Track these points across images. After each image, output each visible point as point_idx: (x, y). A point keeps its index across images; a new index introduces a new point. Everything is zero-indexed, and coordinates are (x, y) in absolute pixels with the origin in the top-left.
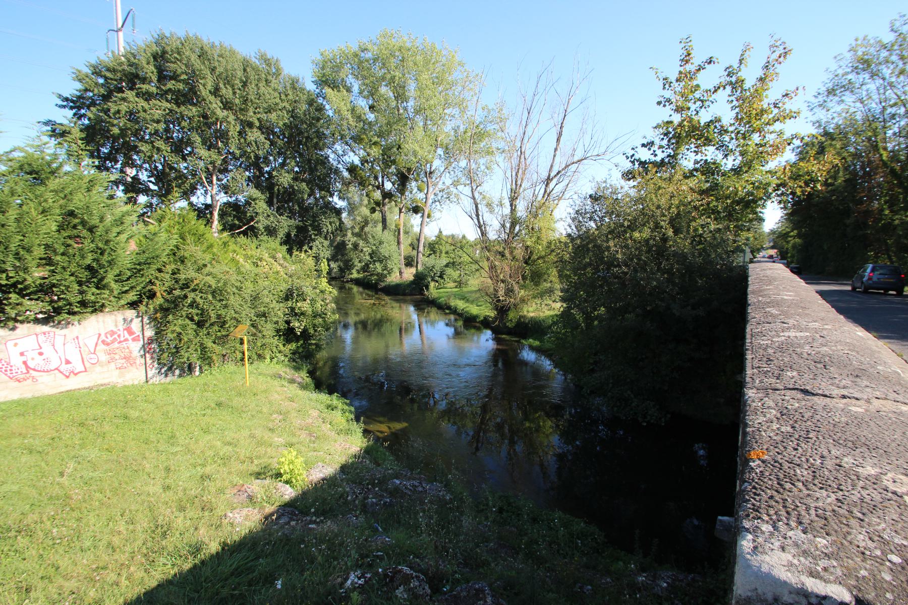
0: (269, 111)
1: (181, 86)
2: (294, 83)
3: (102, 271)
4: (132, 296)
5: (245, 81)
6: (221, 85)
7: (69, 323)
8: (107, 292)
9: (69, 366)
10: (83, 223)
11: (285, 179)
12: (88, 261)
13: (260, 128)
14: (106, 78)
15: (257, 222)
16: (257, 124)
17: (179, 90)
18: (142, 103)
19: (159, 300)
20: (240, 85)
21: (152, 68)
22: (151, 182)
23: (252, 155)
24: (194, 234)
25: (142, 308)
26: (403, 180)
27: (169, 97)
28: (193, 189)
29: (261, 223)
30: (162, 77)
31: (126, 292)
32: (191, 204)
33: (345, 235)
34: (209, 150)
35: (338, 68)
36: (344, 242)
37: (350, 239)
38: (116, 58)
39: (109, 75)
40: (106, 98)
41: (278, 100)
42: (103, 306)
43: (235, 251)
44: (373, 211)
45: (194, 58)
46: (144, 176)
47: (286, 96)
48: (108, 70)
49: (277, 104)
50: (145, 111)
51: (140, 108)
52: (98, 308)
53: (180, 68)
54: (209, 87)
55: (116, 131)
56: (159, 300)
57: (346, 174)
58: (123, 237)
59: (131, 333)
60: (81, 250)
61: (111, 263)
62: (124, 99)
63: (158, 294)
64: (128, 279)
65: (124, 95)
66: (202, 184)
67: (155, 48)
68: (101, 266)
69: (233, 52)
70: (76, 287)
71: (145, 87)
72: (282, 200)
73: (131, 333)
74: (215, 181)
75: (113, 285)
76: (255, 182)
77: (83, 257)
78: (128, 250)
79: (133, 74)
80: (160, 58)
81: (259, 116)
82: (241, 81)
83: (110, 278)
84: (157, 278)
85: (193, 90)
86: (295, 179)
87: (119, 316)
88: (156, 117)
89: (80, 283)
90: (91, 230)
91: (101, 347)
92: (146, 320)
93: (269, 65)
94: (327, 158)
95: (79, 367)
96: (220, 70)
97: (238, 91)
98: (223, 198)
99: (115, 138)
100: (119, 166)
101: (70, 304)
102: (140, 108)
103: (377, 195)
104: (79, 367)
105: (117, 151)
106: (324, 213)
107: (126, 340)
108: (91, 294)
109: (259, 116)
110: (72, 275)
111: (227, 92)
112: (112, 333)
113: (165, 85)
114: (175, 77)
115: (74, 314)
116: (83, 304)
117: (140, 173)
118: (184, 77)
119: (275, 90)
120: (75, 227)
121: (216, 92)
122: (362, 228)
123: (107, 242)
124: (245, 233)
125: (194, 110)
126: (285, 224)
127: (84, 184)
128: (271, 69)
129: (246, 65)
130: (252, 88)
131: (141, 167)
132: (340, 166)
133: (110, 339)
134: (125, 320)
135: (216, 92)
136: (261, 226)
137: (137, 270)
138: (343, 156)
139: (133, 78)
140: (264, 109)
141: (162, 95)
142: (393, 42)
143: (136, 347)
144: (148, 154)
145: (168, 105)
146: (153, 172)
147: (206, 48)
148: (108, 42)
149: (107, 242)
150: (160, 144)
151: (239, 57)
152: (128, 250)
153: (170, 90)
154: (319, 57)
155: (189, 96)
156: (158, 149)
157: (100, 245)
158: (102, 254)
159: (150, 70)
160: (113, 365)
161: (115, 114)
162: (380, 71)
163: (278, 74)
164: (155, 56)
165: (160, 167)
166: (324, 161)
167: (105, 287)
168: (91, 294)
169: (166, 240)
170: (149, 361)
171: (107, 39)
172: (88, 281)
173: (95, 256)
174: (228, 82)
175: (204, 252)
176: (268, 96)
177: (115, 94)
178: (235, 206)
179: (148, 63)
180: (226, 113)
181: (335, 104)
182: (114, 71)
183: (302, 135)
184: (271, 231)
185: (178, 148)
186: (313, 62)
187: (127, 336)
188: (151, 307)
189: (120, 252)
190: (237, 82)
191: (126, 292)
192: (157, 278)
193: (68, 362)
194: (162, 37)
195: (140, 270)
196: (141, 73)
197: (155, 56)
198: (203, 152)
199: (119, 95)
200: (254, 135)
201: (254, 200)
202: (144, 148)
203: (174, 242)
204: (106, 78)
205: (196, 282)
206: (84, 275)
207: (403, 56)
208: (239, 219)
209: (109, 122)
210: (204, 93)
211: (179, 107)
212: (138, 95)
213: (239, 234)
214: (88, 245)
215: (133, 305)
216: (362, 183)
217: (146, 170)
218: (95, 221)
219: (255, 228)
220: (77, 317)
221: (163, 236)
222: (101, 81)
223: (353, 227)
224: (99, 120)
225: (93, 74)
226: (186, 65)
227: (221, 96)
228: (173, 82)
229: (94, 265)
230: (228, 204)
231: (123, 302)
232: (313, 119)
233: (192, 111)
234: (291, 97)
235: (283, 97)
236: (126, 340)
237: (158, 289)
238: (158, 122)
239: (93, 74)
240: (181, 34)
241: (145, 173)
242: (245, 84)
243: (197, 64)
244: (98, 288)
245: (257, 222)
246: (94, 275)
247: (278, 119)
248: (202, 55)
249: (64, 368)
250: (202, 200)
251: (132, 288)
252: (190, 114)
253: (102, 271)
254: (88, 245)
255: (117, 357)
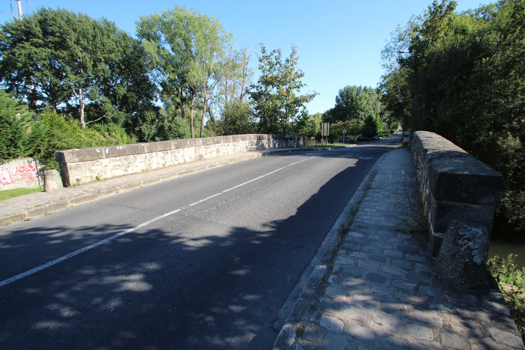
0: (110, 52)
1: (57, 39)
2: (125, 36)
3: (16, 141)
4: (30, 152)
5: (97, 34)
6: (81, 39)
7: (3, 163)
8: (19, 150)
9: (5, 180)
10: (6, 122)
11: (122, 91)
12: (10, 137)
13: (106, 62)
14: (12, 34)
15: (107, 115)
16: (103, 60)
17: (56, 41)
18: (34, 49)
19: (42, 153)
20: (92, 38)
21: (39, 29)
22: (43, 92)
23: (102, 77)
24: (58, 125)
25: (35, 156)
26: (193, 90)
27: (50, 46)
28: (69, 97)
29: (109, 116)
30: (46, 33)
31: (27, 150)
32: (68, 105)
33: (163, 122)
34: (76, 75)
35: (150, 27)
36: (163, 126)
37: (166, 124)
38: (17, 22)
39: (13, 32)
40: (14, 44)
41: (115, 46)
42: (18, 156)
43: (80, 132)
44: (177, 108)
45: (63, 23)
46: (39, 89)
47: (120, 43)
48: (13, 29)
49: (114, 49)
50: (36, 54)
51: (33, 52)
52: (15, 157)
53: (55, 29)
54: (73, 39)
55: (20, 65)
56: (42, 153)
57: (161, 88)
58: (24, 127)
59: (31, 167)
60: (6, 132)
61: (20, 137)
62: (23, 47)
63: (42, 151)
64: (28, 144)
65: (23, 45)
66: (74, 94)
67: (39, 17)
68: (16, 139)
69: (87, 18)
70: (5, 147)
71: (35, 40)
72: (123, 103)
73: (31, 167)
74: (81, 93)
75: (21, 147)
76: (106, 92)
77: (7, 135)
78: (28, 131)
79: (27, 31)
80: (43, 23)
81: (104, 55)
82: (93, 36)
83: (20, 144)
84: (41, 144)
85: (64, 40)
86: (129, 90)
87: (26, 160)
88: (43, 57)
89: (7, 146)
90: (10, 124)
91: (18, 173)
92: (38, 162)
93: (109, 26)
94: (148, 77)
95: (10, 181)
96: (79, 29)
97: (91, 42)
98: (87, 101)
99: (20, 69)
100: (23, 83)
101: (4, 154)
102: (33, 52)
103: (178, 100)
104: (10, 181)
105: (22, 75)
106: (147, 110)
107: (29, 170)
108: (12, 150)
109: (104, 55)
110: (3, 142)
111: (84, 42)
112: (23, 167)
113: (47, 38)
114: (53, 34)
115: (6, 159)
116: (9, 155)
117: (37, 88)
118: (58, 34)
119: (113, 40)
120: (3, 123)
121: (77, 42)
122: (173, 118)
123: (17, 129)
124: (100, 122)
125: (65, 53)
126: (123, 116)
127: (5, 105)
128: (109, 29)
129: (95, 26)
130: (98, 40)
131: (37, 84)
132: (156, 83)
133: (22, 170)
134: (28, 161)
135: (77, 42)
136: (109, 118)
137: (32, 140)
138: (156, 77)
139: (28, 34)
140: (107, 51)
141: (45, 45)
142: (181, 14)
143: (34, 174)
144: (40, 78)
145: (50, 51)
146: (44, 87)
147: (70, 17)
148: (11, 7)
149: (17, 129)
150: (47, 72)
151: (91, 21)
152: (28, 131)
153: (50, 42)
154: (140, 20)
155: (62, 45)
156: (46, 75)
157: (14, 130)
158: (16, 134)
159: (38, 30)
160: (24, 181)
161: (19, 55)
162: (174, 29)
163: (114, 31)
164: (40, 22)
165: (49, 84)
166: (146, 79)
167: (18, 147)
168: (12, 150)
169: (44, 128)
170: (40, 179)
171: (11, 5)
172: (10, 146)
173: (13, 135)
174: (84, 37)
175: (62, 132)
176: (109, 44)
177: (18, 44)
178: (96, 106)
179: (36, 26)
180: (84, 54)
181: (149, 47)
182: (16, 29)
183: (131, 64)
184: (115, 120)
185: (58, 74)
186: (136, 23)
187: (29, 168)
188: (39, 156)
189: (23, 133)
190: (90, 36)
191: (27, 150)
192: (41, 144)
193: (4, 179)
194: (44, 10)
195: (33, 141)
196: (32, 32)
197: (40, 22)
198: (72, 77)
199: (21, 45)
200: (103, 66)
201: (104, 103)
202: (38, 74)
203: (48, 128)
204: (12, 34)
205: (58, 145)
206: (9, 143)
207: (188, 22)
208: (98, 113)
209: (15, 60)
210: (70, 43)
211: (56, 51)
212: (31, 45)
213: (96, 122)
214: (9, 130)
215: (31, 156)
216: (168, 93)
217: (40, 86)
218: (11, 120)
219: (106, 118)
220: (7, 160)
221: (43, 126)
222: (9, 35)
223: (168, 117)
224: (9, 59)
225: (4, 31)
226: (60, 28)
227: (81, 45)
228: (52, 37)
229: (13, 138)
230: (91, 105)
231: (26, 154)
232: (136, 56)
233: (64, 54)
234: (123, 44)
235: (118, 44)
236: (29, 170)
237: (42, 148)
238: (45, 60)
239: (4, 31)
240: (55, 9)
241: (40, 88)
242: (94, 37)
243: (66, 28)
244: (15, 148)
245: (107, 115)
246: (13, 143)
247: (116, 57)
248: (68, 21)
249: (3, 181)
250: (74, 102)
251: (30, 148)
252: (63, 55)
253: (16, 141)
254: (9, 130)
255: (26, 177)
